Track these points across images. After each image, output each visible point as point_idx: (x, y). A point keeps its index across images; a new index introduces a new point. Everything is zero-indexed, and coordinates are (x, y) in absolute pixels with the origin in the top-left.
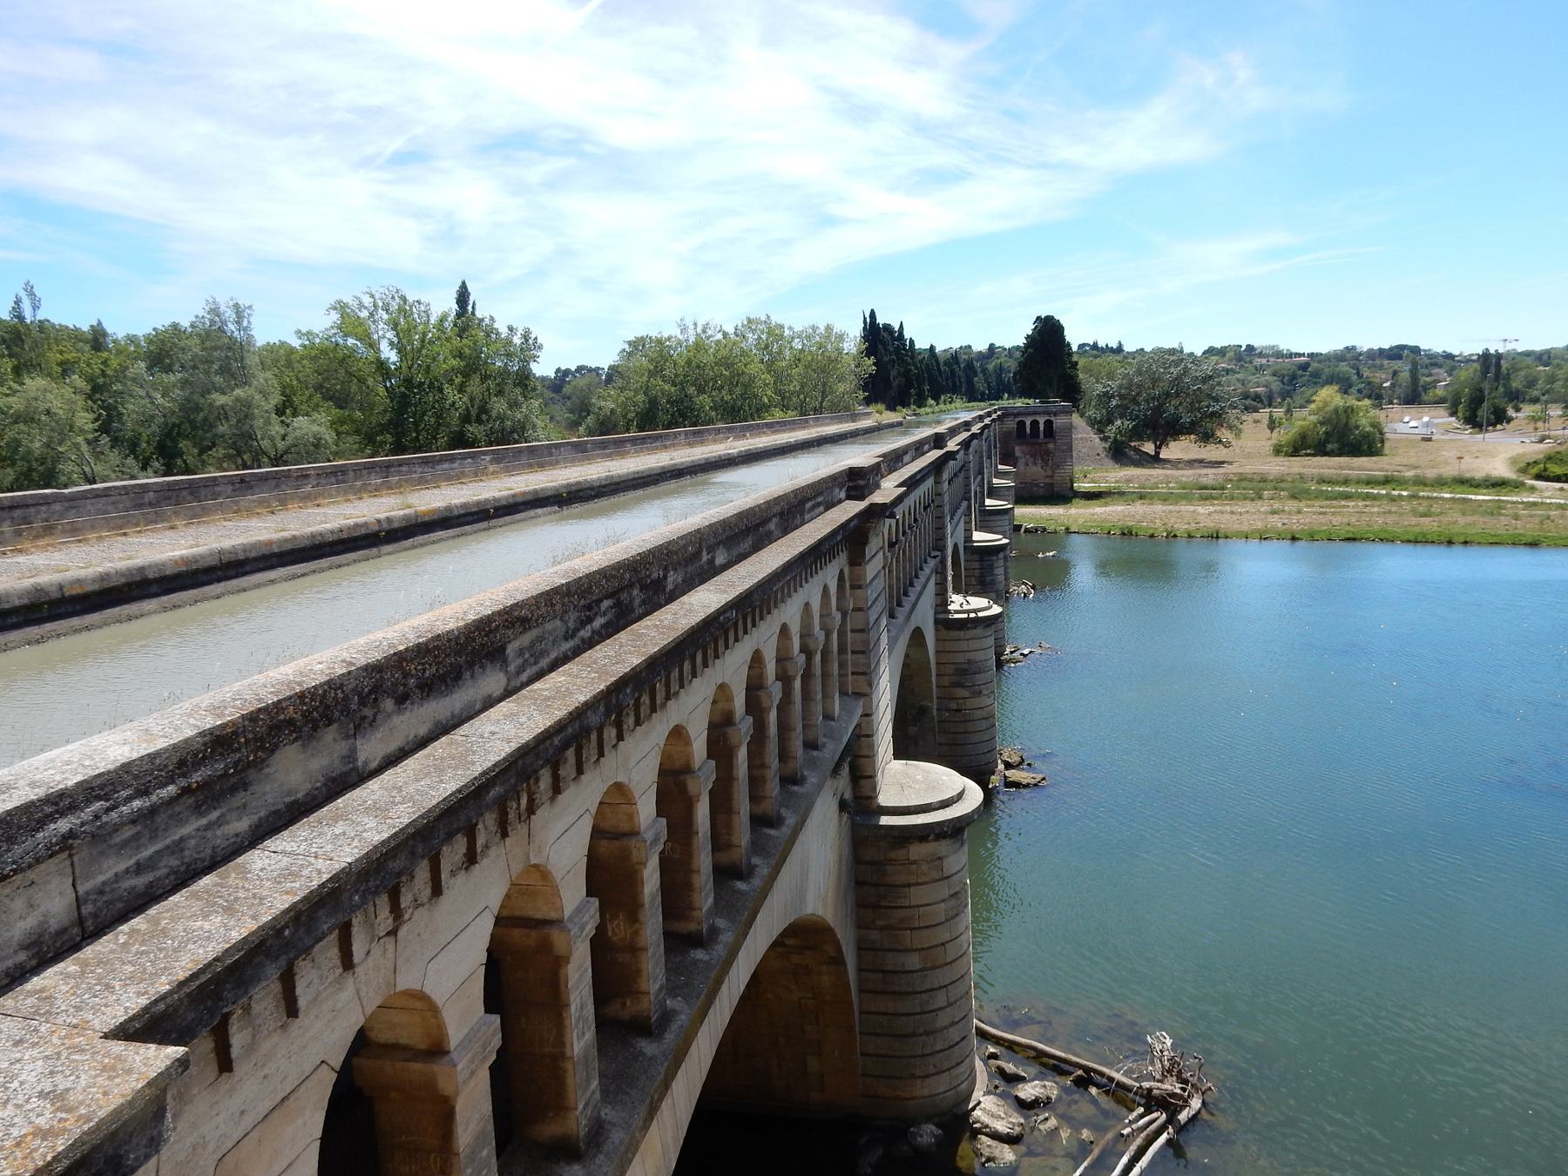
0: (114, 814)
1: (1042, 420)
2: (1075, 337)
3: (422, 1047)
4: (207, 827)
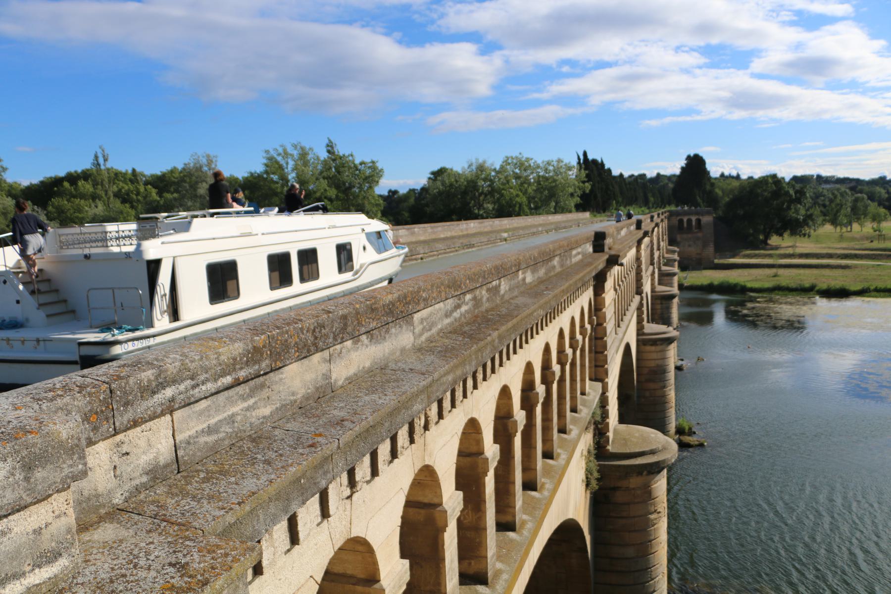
0: (197, 390)
1: (694, 218)
2: (715, 168)
3: (362, 576)
4: (247, 409)
